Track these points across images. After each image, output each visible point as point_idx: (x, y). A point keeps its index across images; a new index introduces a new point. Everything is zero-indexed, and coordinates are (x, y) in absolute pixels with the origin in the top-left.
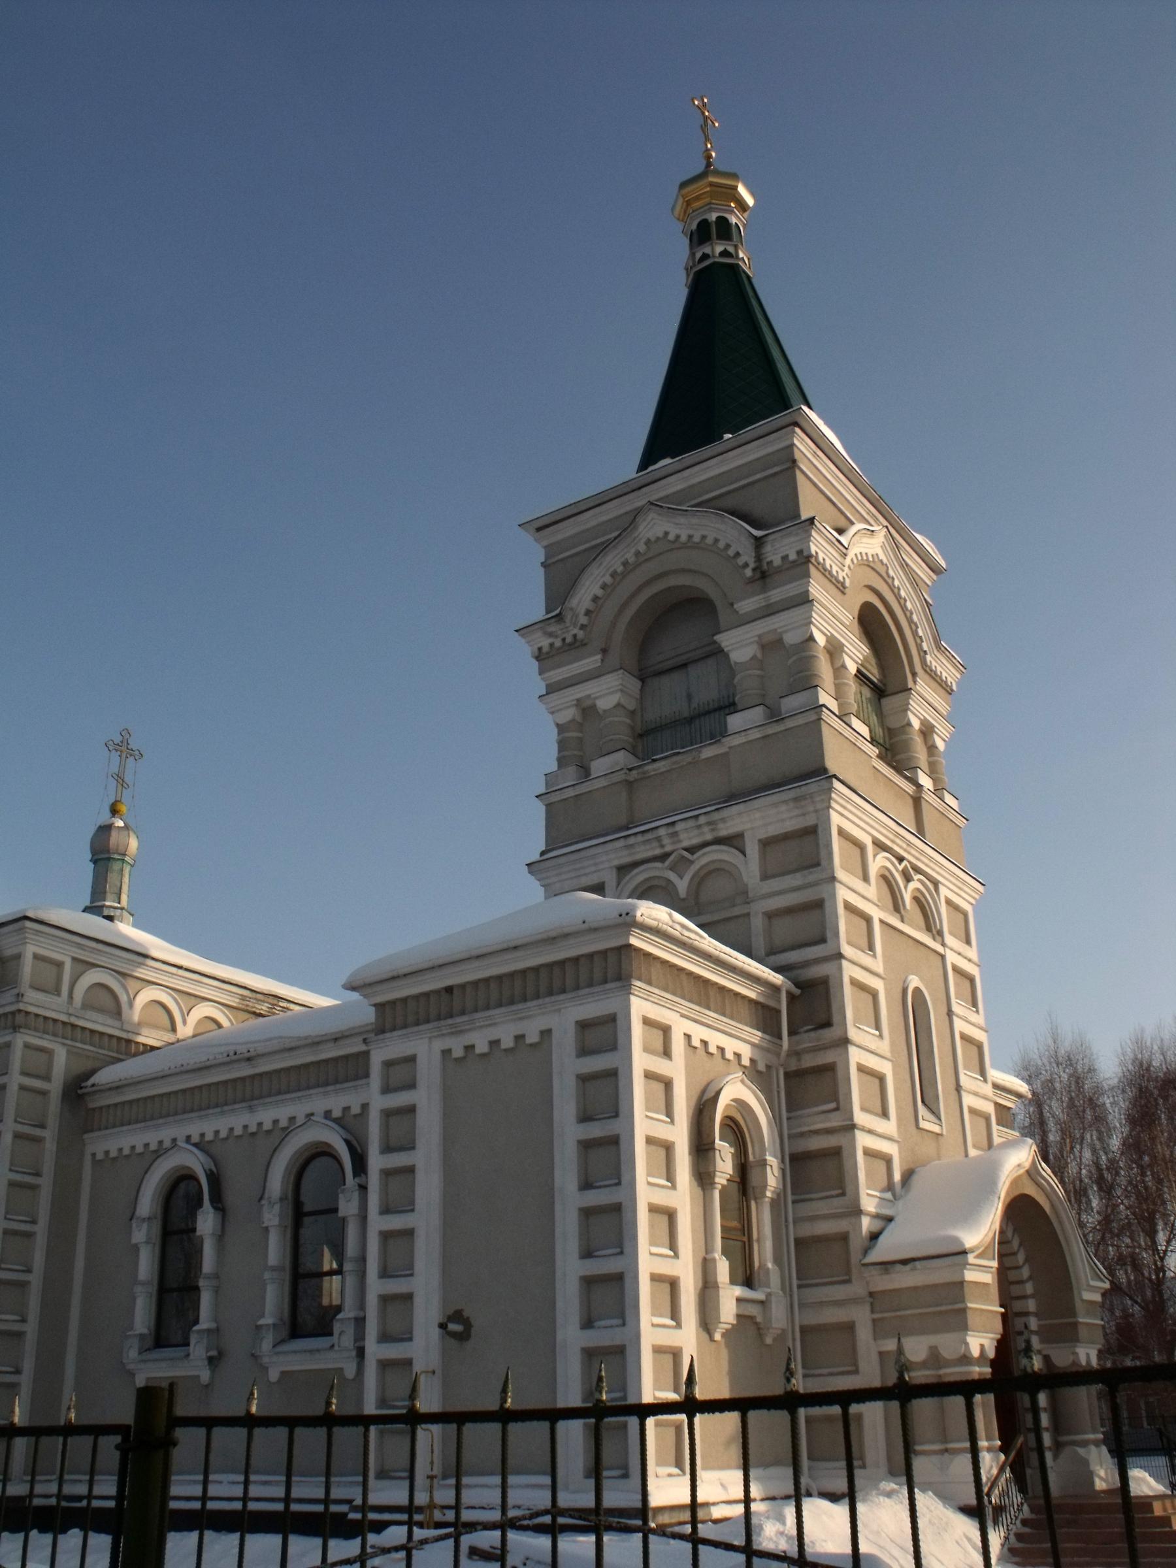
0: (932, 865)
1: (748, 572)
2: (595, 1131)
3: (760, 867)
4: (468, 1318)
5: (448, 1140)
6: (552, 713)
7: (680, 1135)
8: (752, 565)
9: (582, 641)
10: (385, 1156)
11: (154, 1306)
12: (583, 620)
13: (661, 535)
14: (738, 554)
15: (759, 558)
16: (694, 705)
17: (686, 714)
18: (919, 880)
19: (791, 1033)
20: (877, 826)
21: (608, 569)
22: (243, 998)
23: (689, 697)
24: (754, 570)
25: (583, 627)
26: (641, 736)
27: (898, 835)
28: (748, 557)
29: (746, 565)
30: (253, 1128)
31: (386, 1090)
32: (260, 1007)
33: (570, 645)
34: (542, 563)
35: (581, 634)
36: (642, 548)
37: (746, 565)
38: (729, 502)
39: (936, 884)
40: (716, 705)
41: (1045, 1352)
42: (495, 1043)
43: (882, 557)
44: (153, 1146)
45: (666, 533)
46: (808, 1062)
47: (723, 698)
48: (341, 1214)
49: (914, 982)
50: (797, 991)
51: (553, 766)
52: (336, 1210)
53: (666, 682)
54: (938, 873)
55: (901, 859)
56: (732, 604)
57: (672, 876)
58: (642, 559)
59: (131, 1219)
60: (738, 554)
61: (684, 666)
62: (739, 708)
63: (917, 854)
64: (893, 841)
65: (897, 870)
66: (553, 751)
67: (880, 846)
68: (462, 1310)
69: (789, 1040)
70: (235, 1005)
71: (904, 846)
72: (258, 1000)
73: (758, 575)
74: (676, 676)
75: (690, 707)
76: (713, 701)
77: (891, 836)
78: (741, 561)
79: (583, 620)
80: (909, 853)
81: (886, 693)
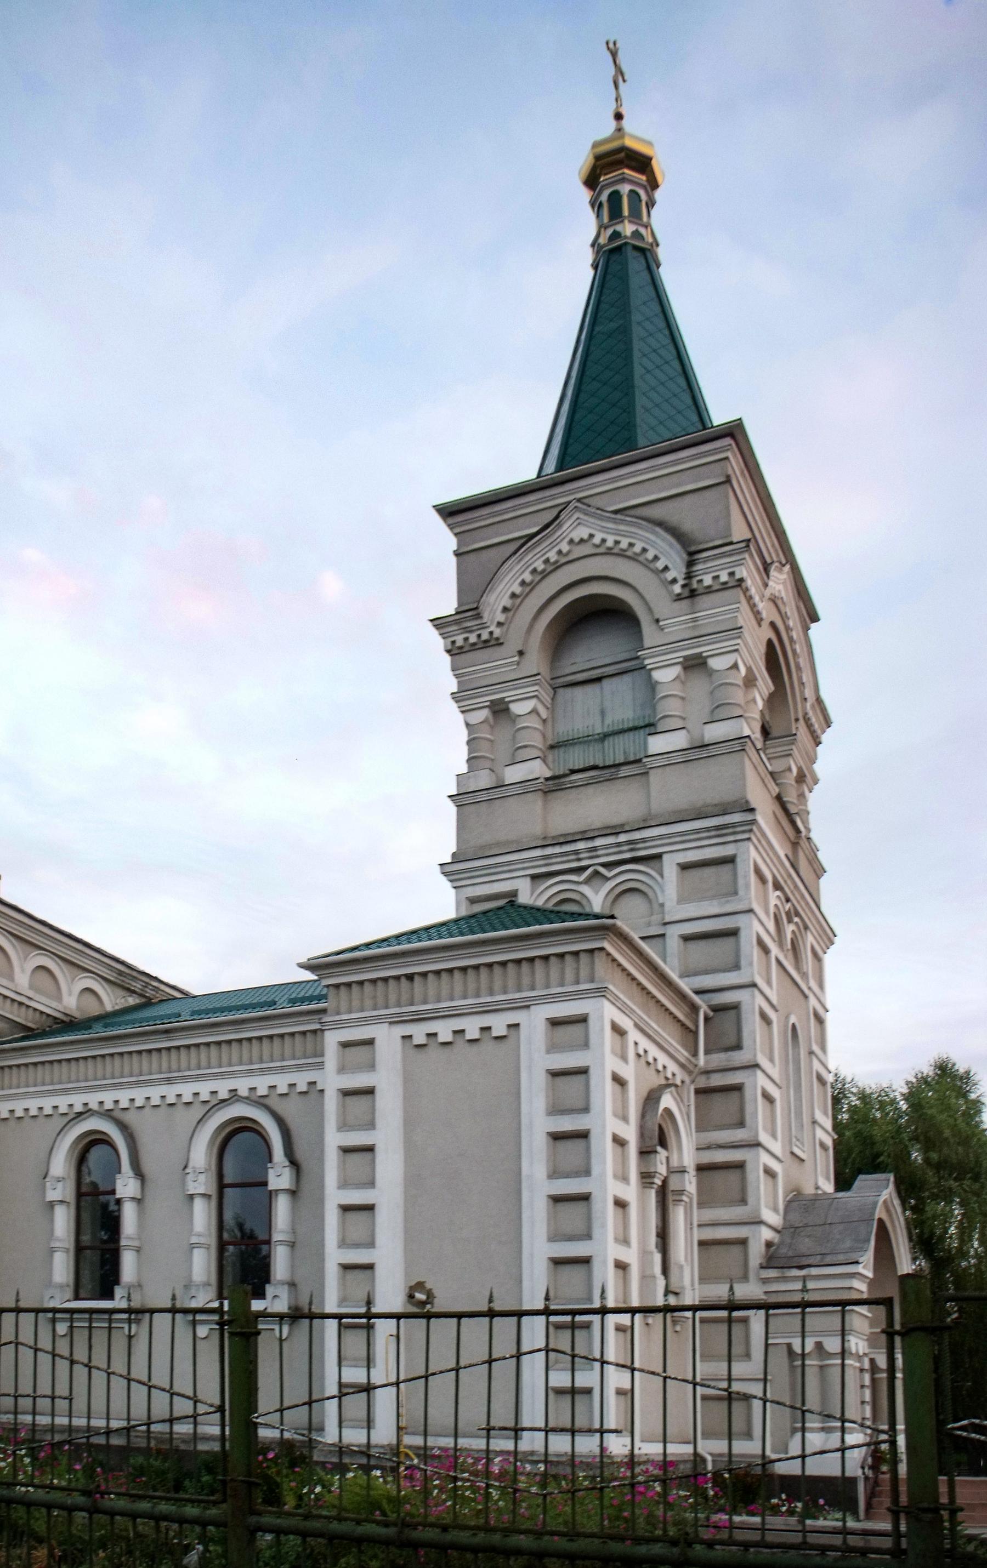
0: (807, 910)
1: (677, 589)
2: (567, 1124)
3: (678, 891)
4: (431, 1289)
5: (410, 1123)
6: (463, 712)
7: (630, 1133)
8: (681, 582)
9: (497, 639)
10: (552, 1118)
11: (72, 1263)
12: (501, 617)
13: (586, 537)
14: (666, 568)
15: (689, 576)
16: (608, 721)
17: (599, 730)
18: (796, 923)
19: (707, 1052)
20: (775, 861)
21: (661, 552)
22: (120, 973)
23: (603, 713)
24: (684, 586)
25: (500, 624)
26: (552, 747)
27: (790, 876)
28: (676, 573)
29: (674, 581)
30: (171, 1099)
31: (342, 1070)
32: (135, 984)
33: (486, 641)
34: (454, 551)
35: (497, 632)
36: (565, 547)
37: (674, 581)
38: (656, 512)
39: (806, 928)
40: (631, 725)
41: (872, 1356)
42: (459, 1033)
43: (783, 594)
44: (78, 1108)
45: (591, 536)
46: (717, 1080)
47: (628, 719)
48: (271, 1187)
49: (793, 1019)
50: (711, 1014)
51: (464, 769)
52: (265, 1184)
53: (578, 693)
54: (809, 919)
55: (788, 900)
56: (657, 621)
57: (585, 889)
58: (564, 560)
59: (45, 1178)
60: (666, 568)
61: (599, 680)
62: (660, 729)
63: (798, 897)
64: (785, 882)
65: (784, 908)
66: (463, 753)
67: (777, 886)
68: (424, 1282)
69: (705, 1059)
70: (112, 979)
71: (792, 887)
72: (134, 978)
73: (686, 593)
74: (591, 690)
75: (603, 722)
76: (628, 719)
77: (785, 876)
78: (670, 576)
79: (501, 617)
80: (794, 895)
81: (770, 736)
